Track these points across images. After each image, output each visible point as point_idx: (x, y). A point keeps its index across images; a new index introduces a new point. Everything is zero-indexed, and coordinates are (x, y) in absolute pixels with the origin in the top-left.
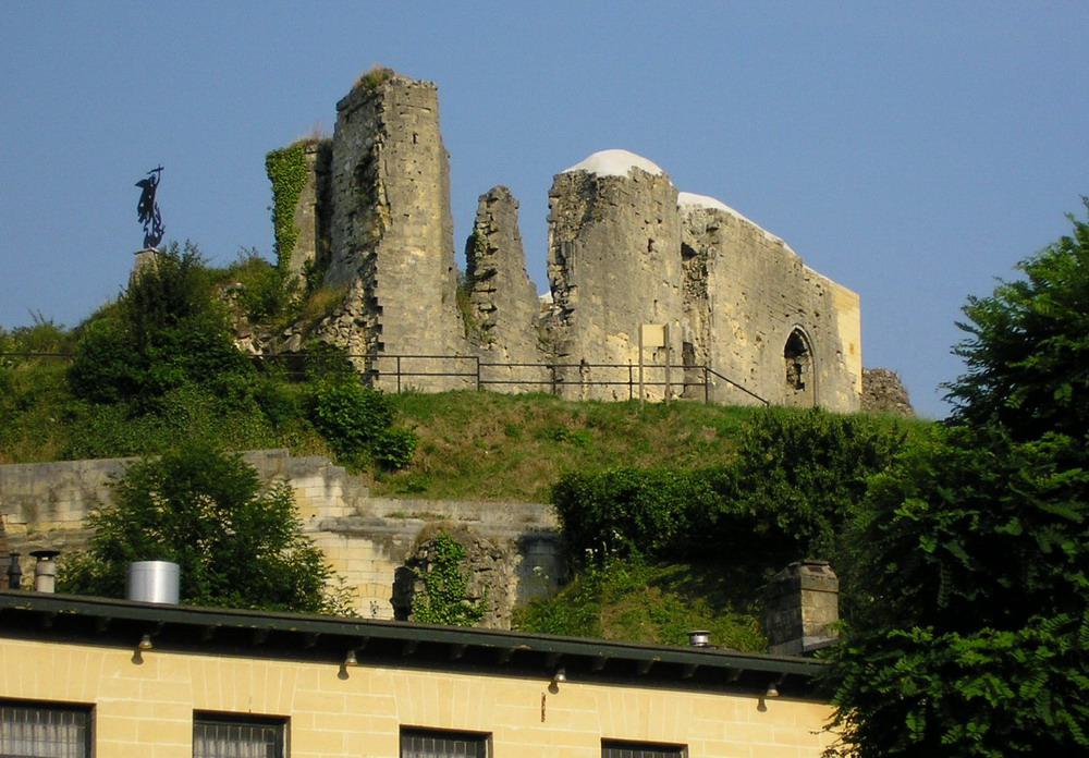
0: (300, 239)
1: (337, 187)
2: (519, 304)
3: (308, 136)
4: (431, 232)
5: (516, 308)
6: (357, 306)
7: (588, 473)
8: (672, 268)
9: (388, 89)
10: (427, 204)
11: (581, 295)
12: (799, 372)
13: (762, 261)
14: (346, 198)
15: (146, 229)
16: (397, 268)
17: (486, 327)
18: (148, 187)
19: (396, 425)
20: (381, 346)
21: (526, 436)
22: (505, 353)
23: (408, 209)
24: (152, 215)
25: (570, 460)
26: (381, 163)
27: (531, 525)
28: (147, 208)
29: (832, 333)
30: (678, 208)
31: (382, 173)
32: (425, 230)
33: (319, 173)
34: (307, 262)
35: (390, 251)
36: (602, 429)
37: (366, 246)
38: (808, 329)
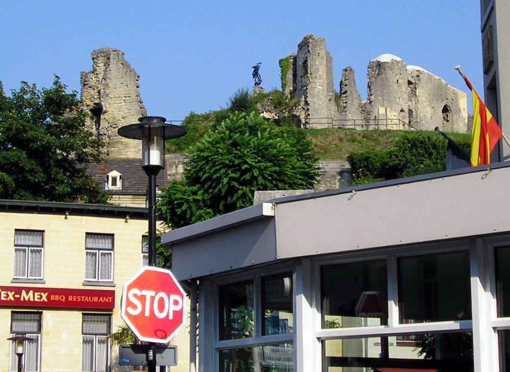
0: (289, 84)
1: (298, 68)
2: (355, 100)
3: (291, 55)
4: (324, 81)
5: (354, 102)
6: (302, 103)
7: (357, 152)
8: (405, 88)
9: (311, 40)
10: (322, 73)
11: (375, 97)
12: (447, 117)
13: (434, 85)
14: (300, 72)
15: (255, 80)
16: (314, 92)
17: (345, 108)
18: (256, 69)
19: (307, 139)
20: (309, 115)
21: (345, 141)
22: (350, 115)
23: (317, 75)
24: (257, 76)
25: (357, 148)
26: (309, 62)
27: (343, 167)
28: (256, 73)
29: (457, 105)
30: (406, 70)
31: (309, 65)
32: (322, 81)
33: (293, 65)
34: (290, 91)
35: (312, 87)
36: (367, 138)
37: (305, 86)
38: (449, 104)
